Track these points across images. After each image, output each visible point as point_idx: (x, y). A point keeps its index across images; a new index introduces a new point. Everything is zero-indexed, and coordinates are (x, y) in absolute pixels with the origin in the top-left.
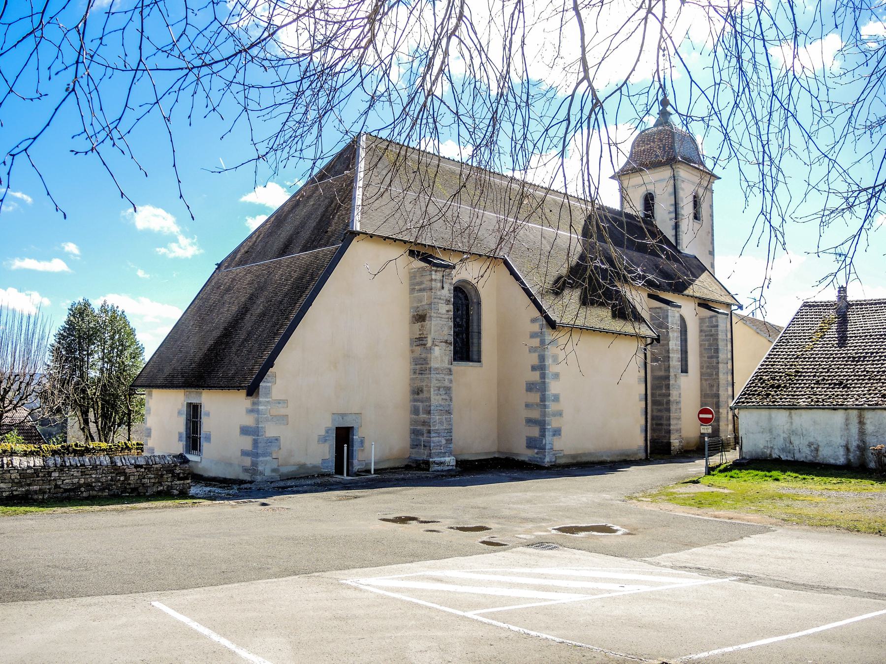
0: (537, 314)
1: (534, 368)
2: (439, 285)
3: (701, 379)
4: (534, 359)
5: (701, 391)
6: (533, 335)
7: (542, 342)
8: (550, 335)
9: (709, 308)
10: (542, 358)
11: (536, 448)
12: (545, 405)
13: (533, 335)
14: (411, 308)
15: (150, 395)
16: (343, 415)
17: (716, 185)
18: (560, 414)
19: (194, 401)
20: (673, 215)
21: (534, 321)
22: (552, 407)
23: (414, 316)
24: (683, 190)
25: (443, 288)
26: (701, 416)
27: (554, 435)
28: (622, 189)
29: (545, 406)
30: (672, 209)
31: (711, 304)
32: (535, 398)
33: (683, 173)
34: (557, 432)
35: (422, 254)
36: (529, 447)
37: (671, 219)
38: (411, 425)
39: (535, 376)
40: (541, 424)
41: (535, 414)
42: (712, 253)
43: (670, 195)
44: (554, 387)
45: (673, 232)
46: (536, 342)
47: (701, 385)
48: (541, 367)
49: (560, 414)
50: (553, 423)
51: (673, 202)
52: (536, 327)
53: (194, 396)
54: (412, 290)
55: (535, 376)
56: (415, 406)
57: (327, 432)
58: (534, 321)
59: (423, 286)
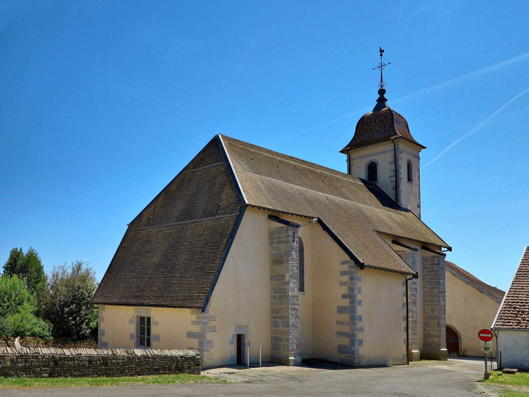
0: (347, 258)
1: (344, 297)
2: (292, 239)
3: (424, 305)
4: (344, 290)
5: (424, 314)
6: (343, 273)
7: (352, 278)
8: (360, 273)
9: (429, 250)
10: (351, 290)
11: (346, 353)
12: (354, 323)
13: (343, 273)
14: (271, 255)
15: (104, 310)
16: (240, 327)
17: (422, 153)
18: (362, 330)
19: (146, 315)
20: (394, 179)
21: (343, 263)
22: (359, 325)
23: (273, 260)
24: (401, 159)
25: (294, 241)
26: (481, 335)
27: (359, 344)
28: (349, 161)
29: (354, 324)
30: (393, 174)
31: (430, 247)
32: (345, 317)
33: (402, 146)
34: (361, 343)
35: (274, 216)
36: (133, 339)
37: (391, 182)
38: (271, 334)
39: (346, 302)
40: (352, 337)
41: (347, 329)
42: (419, 206)
43: (353, 165)
44: (360, 311)
45: (394, 192)
46: (346, 278)
47: (424, 309)
48: (351, 296)
49: (362, 330)
50: (360, 336)
51: (394, 168)
52: (346, 268)
53: (144, 311)
54: (271, 243)
55: (346, 302)
56: (275, 321)
57: (233, 338)
58: (343, 263)
59: (282, 239)
